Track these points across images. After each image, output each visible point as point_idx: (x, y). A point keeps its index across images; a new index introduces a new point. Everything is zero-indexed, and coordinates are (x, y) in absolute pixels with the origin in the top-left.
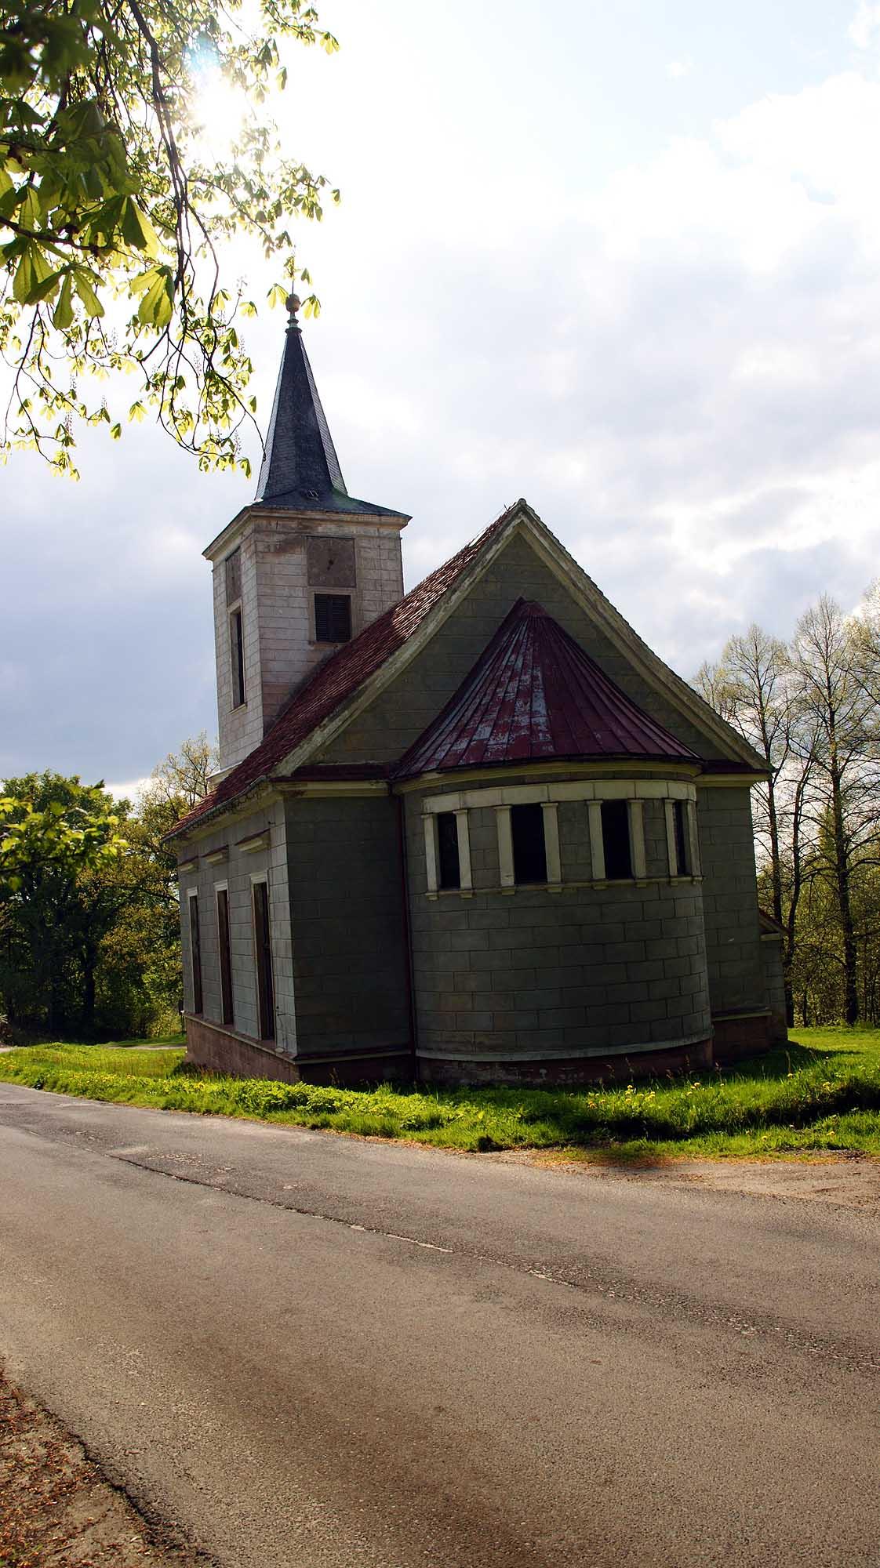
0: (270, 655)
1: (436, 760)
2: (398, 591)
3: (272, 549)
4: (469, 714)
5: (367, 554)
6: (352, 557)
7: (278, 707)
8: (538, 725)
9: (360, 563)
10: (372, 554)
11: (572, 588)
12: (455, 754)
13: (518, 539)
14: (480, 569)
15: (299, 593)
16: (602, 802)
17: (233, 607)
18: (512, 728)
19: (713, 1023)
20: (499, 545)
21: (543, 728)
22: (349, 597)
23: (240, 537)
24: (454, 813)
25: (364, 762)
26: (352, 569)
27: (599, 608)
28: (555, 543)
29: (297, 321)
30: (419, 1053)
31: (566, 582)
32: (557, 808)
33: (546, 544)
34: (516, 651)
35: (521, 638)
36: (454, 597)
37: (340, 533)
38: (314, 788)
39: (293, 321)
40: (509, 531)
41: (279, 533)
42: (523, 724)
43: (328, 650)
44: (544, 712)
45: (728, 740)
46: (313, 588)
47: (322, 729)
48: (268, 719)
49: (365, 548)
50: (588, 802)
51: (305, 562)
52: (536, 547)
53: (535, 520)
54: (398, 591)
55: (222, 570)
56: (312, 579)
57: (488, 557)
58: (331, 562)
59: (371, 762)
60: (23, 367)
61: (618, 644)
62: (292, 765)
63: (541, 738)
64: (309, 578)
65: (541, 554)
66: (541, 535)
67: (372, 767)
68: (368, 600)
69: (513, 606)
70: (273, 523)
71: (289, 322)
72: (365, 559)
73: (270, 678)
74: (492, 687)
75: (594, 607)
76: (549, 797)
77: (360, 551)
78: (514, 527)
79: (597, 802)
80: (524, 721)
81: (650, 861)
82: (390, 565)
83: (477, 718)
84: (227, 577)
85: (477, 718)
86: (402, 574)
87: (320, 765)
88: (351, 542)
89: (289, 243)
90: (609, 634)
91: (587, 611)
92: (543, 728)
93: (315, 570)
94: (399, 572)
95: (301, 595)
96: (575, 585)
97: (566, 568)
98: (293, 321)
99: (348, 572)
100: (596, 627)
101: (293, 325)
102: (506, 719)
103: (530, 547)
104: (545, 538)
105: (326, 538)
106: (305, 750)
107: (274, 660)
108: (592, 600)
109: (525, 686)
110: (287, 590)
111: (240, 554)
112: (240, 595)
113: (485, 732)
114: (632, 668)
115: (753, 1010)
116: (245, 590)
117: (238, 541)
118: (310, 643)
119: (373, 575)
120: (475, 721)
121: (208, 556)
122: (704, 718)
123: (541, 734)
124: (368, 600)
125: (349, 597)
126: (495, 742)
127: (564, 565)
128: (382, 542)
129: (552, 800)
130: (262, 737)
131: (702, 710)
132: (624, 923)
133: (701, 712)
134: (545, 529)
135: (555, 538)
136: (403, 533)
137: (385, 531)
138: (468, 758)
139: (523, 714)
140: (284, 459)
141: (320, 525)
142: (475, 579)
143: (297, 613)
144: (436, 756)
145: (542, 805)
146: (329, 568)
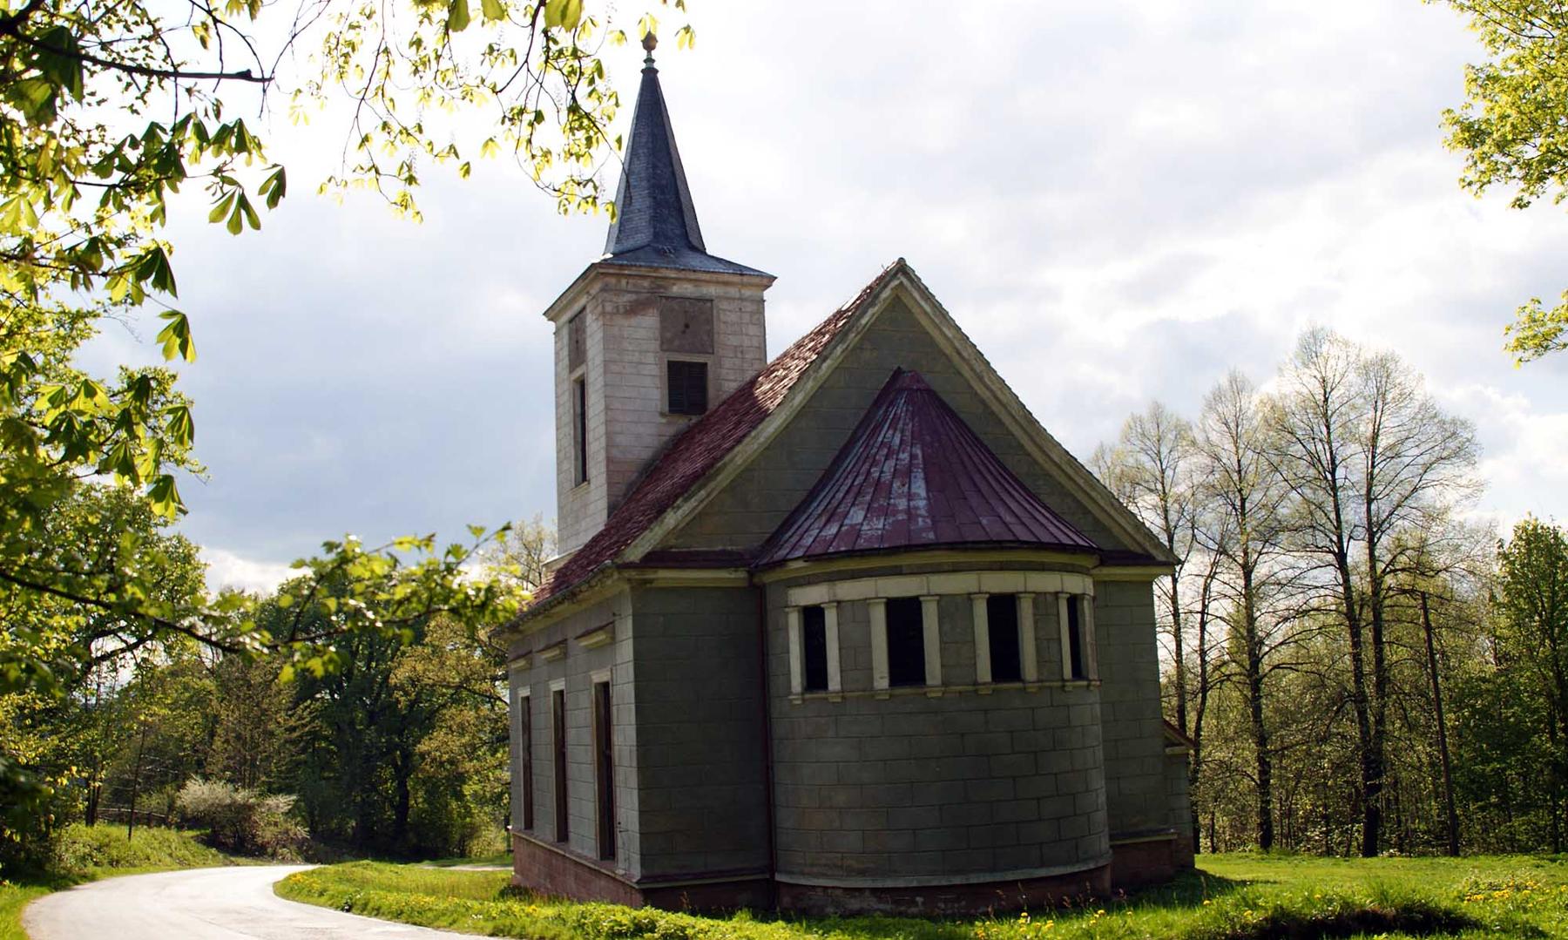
3: (622, 310)
4: (840, 495)
5: (727, 315)
6: (709, 321)
7: (624, 488)
8: (917, 508)
9: (719, 327)
10: (733, 317)
11: (956, 359)
15: (650, 358)
16: (987, 596)
17: (578, 373)
18: (887, 511)
19: (1111, 847)
20: (876, 308)
21: (923, 512)
26: (710, 333)
28: (937, 307)
29: (653, 61)
33: (928, 309)
34: (893, 426)
36: (825, 366)
38: (665, 576)
39: (649, 60)
40: (886, 293)
43: (682, 423)
44: (923, 493)
45: (1129, 529)
50: (972, 596)
52: (916, 310)
55: (565, 332)
56: (665, 344)
57: (863, 321)
58: (687, 326)
59: (729, 548)
61: (1007, 420)
64: (662, 343)
65: (924, 322)
66: (922, 298)
73: (615, 452)
74: (867, 466)
76: (928, 587)
80: (902, 504)
81: (1041, 662)
82: (753, 330)
83: (849, 499)
84: (570, 338)
85: (849, 499)
88: (709, 304)
90: (995, 407)
93: (668, 335)
96: (959, 353)
97: (950, 335)
98: (649, 60)
99: (705, 338)
100: (983, 402)
113: (857, 516)
117: (583, 301)
118: (662, 415)
119: (733, 341)
122: (1102, 504)
123: (920, 519)
125: (706, 364)
127: (947, 332)
129: (932, 593)
136: (767, 294)
137: (747, 292)
139: (900, 496)
141: (674, 284)
143: (648, 382)
145: (921, 599)
146: (684, 332)
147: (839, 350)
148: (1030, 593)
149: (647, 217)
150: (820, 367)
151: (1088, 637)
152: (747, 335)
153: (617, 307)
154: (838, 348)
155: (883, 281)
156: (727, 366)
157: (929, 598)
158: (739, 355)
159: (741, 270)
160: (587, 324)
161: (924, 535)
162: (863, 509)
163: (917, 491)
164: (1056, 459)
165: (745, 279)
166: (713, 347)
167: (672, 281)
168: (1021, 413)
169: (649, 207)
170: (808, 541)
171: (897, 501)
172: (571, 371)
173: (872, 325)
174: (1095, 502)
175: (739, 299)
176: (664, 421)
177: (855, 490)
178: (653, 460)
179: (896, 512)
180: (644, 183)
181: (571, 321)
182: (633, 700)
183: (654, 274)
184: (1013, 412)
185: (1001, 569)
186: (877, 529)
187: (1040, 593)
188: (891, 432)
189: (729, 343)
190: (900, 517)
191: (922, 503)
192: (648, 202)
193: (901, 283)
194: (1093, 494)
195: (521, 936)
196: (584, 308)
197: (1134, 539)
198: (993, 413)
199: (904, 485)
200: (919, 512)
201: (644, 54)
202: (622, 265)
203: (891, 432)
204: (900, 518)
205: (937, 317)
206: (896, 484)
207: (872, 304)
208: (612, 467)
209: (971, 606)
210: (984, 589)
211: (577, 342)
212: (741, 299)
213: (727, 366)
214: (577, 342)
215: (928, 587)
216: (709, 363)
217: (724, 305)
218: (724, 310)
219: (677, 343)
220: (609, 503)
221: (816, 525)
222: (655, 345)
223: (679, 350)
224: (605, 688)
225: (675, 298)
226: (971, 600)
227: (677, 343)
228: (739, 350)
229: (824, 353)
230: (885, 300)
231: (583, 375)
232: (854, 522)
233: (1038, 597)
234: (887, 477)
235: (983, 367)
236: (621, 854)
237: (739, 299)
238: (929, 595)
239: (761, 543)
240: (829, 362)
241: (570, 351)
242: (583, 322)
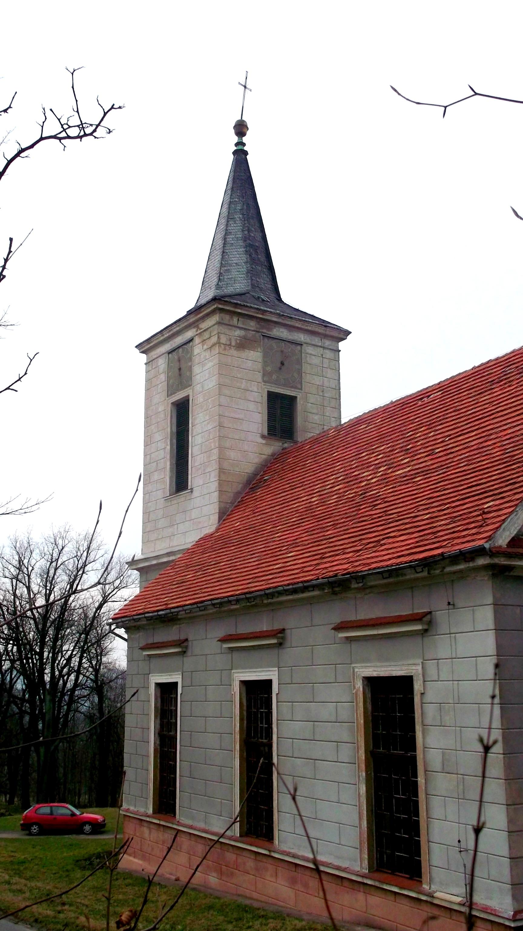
0: (228, 444)
2: (336, 399)
3: (233, 343)
6: (299, 362)
7: (232, 495)
9: (306, 368)
10: (316, 361)
17: (179, 396)
22: (296, 397)
23: (195, 330)
26: (300, 372)
29: (244, 145)
39: (240, 144)
43: (276, 446)
48: (223, 505)
49: (311, 354)
51: (260, 360)
54: (336, 399)
55: (162, 363)
56: (267, 376)
58: (282, 364)
60: (77, 113)
64: (264, 375)
71: (237, 145)
73: (226, 465)
77: (306, 357)
82: (330, 373)
89: (114, 105)
93: (269, 369)
95: (256, 390)
98: (240, 144)
99: (296, 375)
101: (240, 147)
110: (244, 383)
112: (190, 385)
117: (189, 334)
118: (263, 437)
119: (317, 380)
121: (141, 350)
125: (296, 397)
130: (217, 522)
136: (342, 345)
137: (327, 343)
140: (234, 265)
143: (252, 406)
146: (280, 369)
149: (244, 270)
153: (230, 340)
156: (312, 401)
159: (324, 324)
166: (301, 384)
169: (246, 263)
172: (170, 394)
176: (264, 442)
178: (255, 474)
180: (241, 243)
183: (261, 316)
189: (313, 382)
192: (244, 257)
195: (348, 929)
196: (191, 340)
201: (236, 139)
202: (237, 304)
208: (224, 477)
211: (180, 369)
213: (312, 401)
214: (180, 369)
216: (298, 397)
217: (310, 350)
219: (274, 377)
220: (220, 509)
222: (259, 377)
223: (277, 383)
227: (274, 377)
228: (321, 389)
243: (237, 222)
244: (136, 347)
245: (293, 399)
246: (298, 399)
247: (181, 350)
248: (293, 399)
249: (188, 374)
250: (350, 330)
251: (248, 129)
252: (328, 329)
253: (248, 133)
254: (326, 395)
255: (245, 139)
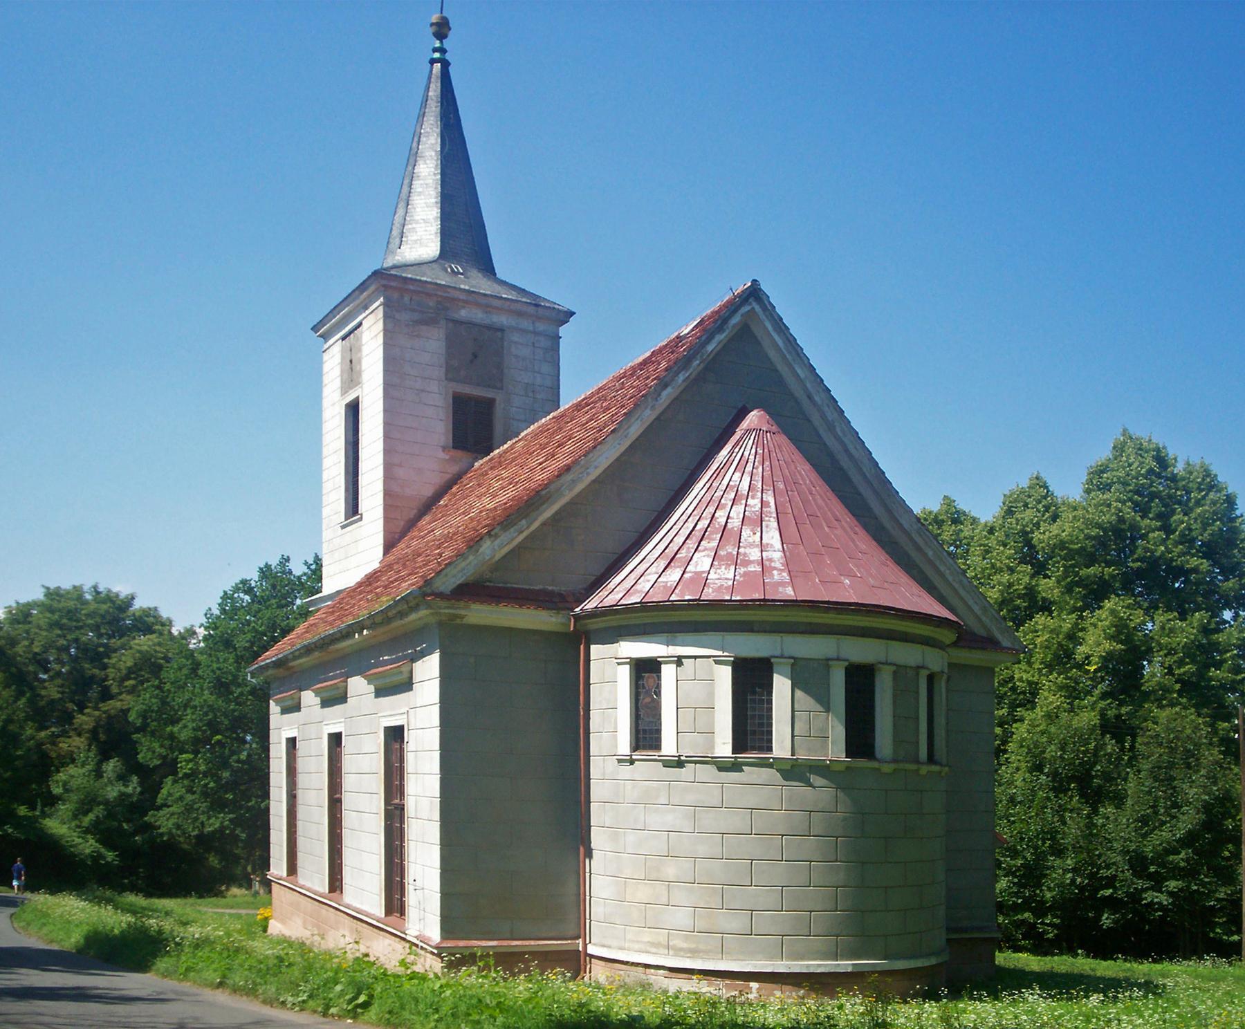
1: (639, 592)
2: (553, 401)
4: (680, 540)
5: (519, 349)
8: (771, 560)
11: (806, 403)
12: (665, 587)
13: (745, 332)
14: (698, 362)
15: (434, 387)
16: (847, 664)
17: (350, 397)
18: (736, 561)
19: (948, 940)
20: (724, 335)
21: (778, 565)
24: (659, 659)
25: (541, 587)
27: (838, 430)
28: (791, 342)
30: (591, 950)
31: (799, 393)
32: (793, 665)
33: (780, 343)
34: (742, 470)
35: (746, 453)
36: (665, 393)
37: (487, 321)
38: (480, 614)
40: (736, 319)
41: (413, 310)
42: (752, 558)
44: (778, 545)
45: (976, 608)
46: (453, 384)
47: (492, 539)
50: (830, 663)
52: (766, 344)
53: (769, 310)
56: (451, 373)
57: (710, 348)
58: (475, 356)
59: (550, 588)
61: (856, 478)
62: (453, 580)
63: (775, 577)
64: (447, 372)
65: (772, 354)
66: (775, 330)
67: (552, 593)
68: (517, 407)
69: (733, 414)
70: (407, 299)
72: (516, 356)
74: (711, 509)
75: (831, 427)
76: (782, 649)
78: (742, 315)
79: (842, 662)
80: (754, 554)
81: (897, 740)
82: (546, 368)
83: (691, 544)
84: (343, 358)
85: (691, 544)
86: (559, 380)
87: (488, 584)
88: (499, 334)
90: (845, 463)
91: (821, 432)
92: (778, 565)
94: (556, 378)
95: (437, 391)
96: (810, 397)
97: (802, 375)
100: (831, 456)
102: (730, 550)
103: (759, 343)
104: (779, 334)
105: (471, 324)
106: (470, 563)
107: (400, 465)
108: (830, 419)
109: (753, 512)
111: (362, 332)
113: (702, 562)
114: (870, 510)
115: (980, 929)
116: (365, 377)
118: (444, 448)
120: (688, 548)
122: (950, 578)
123: (775, 572)
124: (517, 407)
126: (717, 576)
127: (799, 371)
128: (536, 338)
129: (786, 654)
131: (950, 569)
132: (863, 814)
133: (948, 572)
134: (780, 323)
135: (791, 335)
136: (563, 331)
138: (682, 593)
139: (751, 545)
141: (464, 307)
142: (691, 374)
144: (638, 587)
145: (772, 660)
147: (681, 377)
148: (890, 664)
150: (659, 395)
151: (940, 721)
152: (539, 373)
154: (680, 375)
155: (732, 307)
157: (782, 660)
158: (531, 394)
160: (364, 342)
161: (781, 589)
162: (708, 556)
163: (771, 542)
164: (906, 526)
165: (540, 311)
166: (501, 381)
167: (460, 304)
168: (873, 471)
170: (644, 585)
171: (748, 551)
173: (717, 354)
174: (942, 575)
175: (531, 332)
177: (698, 534)
179: (747, 563)
181: (343, 338)
182: (437, 747)
184: (865, 470)
185: (863, 636)
186: (726, 579)
187: (901, 666)
188: (738, 475)
190: (752, 568)
191: (777, 555)
193: (753, 308)
194: (942, 568)
197: (980, 620)
198: (841, 469)
199: (755, 534)
200: (773, 564)
203: (738, 475)
204: (753, 569)
205: (790, 353)
206: (746, 532)
207: (720, 329)
209: (829, 672)
210: (843, 655)
211: (351, 361)
212: (535, 333)
214: (351, 361)
215: (782, 649)
217: (516, 337)
218: (516, 343)
220: (385, 541)
221: (653, 569)
222: (439, 373)
224: (395, 735)
225: (462, 323)
226: (828, 667)
229: (666, 379)
230: (734, 326)
231: (357, 399)
232: (699, 569)
233: (900, 671)
234: (735, 523)
235: (836, 415)
236: (412, 911)
237: (531, 332)
238: (782, 657)
239: (585, 586)
240: (669, 390)
241: (342, 371)
242: (358, 339)
243: (428, 162)
244: (312, 329)
245: (490, 403)
246: (497, 402)
247: (352, 335)
248: (490, 403)
249: (358, 368)
250: (573, 310)
251: (450, 29)
252: (539, 309)
253: (451, 34)
254: (539, 397)
255: (447, 44)
